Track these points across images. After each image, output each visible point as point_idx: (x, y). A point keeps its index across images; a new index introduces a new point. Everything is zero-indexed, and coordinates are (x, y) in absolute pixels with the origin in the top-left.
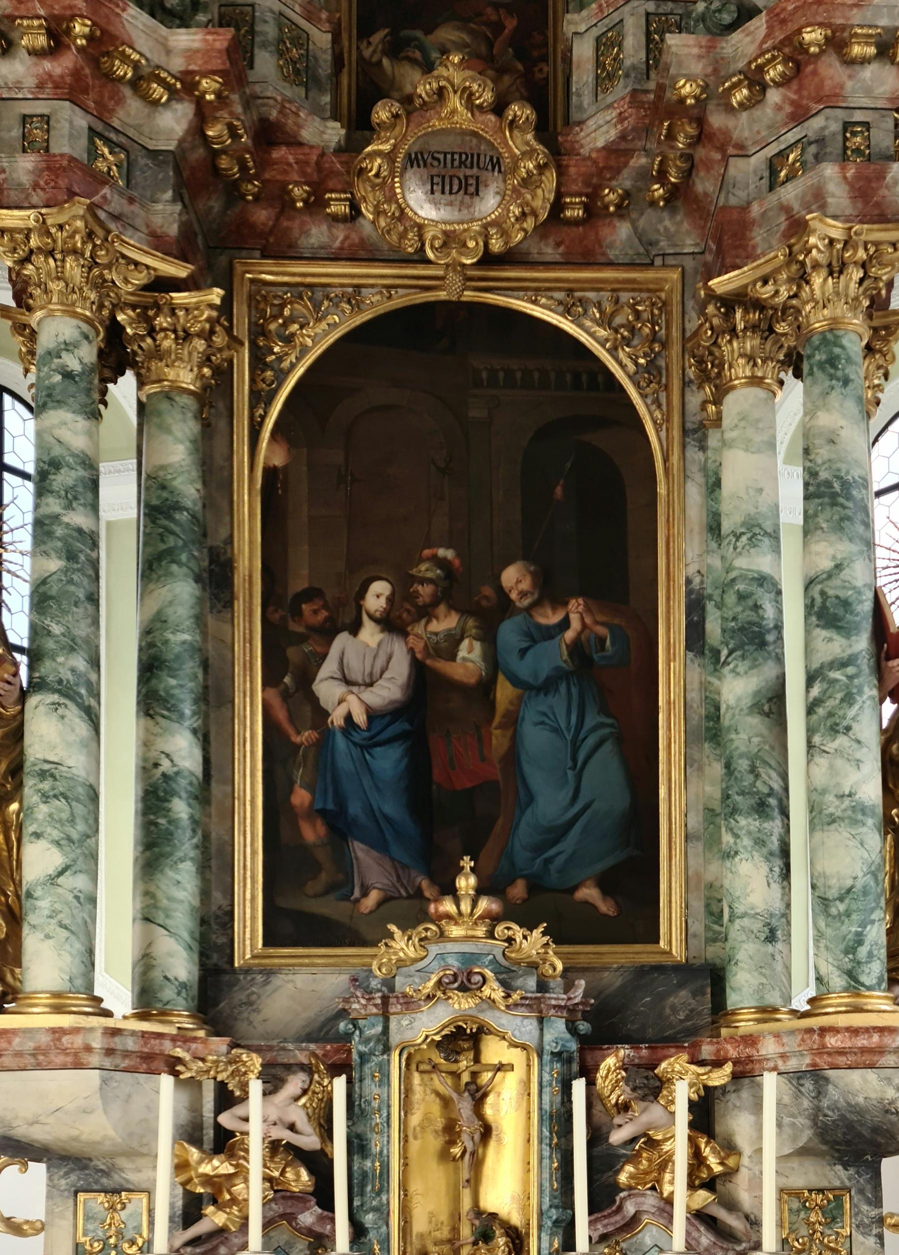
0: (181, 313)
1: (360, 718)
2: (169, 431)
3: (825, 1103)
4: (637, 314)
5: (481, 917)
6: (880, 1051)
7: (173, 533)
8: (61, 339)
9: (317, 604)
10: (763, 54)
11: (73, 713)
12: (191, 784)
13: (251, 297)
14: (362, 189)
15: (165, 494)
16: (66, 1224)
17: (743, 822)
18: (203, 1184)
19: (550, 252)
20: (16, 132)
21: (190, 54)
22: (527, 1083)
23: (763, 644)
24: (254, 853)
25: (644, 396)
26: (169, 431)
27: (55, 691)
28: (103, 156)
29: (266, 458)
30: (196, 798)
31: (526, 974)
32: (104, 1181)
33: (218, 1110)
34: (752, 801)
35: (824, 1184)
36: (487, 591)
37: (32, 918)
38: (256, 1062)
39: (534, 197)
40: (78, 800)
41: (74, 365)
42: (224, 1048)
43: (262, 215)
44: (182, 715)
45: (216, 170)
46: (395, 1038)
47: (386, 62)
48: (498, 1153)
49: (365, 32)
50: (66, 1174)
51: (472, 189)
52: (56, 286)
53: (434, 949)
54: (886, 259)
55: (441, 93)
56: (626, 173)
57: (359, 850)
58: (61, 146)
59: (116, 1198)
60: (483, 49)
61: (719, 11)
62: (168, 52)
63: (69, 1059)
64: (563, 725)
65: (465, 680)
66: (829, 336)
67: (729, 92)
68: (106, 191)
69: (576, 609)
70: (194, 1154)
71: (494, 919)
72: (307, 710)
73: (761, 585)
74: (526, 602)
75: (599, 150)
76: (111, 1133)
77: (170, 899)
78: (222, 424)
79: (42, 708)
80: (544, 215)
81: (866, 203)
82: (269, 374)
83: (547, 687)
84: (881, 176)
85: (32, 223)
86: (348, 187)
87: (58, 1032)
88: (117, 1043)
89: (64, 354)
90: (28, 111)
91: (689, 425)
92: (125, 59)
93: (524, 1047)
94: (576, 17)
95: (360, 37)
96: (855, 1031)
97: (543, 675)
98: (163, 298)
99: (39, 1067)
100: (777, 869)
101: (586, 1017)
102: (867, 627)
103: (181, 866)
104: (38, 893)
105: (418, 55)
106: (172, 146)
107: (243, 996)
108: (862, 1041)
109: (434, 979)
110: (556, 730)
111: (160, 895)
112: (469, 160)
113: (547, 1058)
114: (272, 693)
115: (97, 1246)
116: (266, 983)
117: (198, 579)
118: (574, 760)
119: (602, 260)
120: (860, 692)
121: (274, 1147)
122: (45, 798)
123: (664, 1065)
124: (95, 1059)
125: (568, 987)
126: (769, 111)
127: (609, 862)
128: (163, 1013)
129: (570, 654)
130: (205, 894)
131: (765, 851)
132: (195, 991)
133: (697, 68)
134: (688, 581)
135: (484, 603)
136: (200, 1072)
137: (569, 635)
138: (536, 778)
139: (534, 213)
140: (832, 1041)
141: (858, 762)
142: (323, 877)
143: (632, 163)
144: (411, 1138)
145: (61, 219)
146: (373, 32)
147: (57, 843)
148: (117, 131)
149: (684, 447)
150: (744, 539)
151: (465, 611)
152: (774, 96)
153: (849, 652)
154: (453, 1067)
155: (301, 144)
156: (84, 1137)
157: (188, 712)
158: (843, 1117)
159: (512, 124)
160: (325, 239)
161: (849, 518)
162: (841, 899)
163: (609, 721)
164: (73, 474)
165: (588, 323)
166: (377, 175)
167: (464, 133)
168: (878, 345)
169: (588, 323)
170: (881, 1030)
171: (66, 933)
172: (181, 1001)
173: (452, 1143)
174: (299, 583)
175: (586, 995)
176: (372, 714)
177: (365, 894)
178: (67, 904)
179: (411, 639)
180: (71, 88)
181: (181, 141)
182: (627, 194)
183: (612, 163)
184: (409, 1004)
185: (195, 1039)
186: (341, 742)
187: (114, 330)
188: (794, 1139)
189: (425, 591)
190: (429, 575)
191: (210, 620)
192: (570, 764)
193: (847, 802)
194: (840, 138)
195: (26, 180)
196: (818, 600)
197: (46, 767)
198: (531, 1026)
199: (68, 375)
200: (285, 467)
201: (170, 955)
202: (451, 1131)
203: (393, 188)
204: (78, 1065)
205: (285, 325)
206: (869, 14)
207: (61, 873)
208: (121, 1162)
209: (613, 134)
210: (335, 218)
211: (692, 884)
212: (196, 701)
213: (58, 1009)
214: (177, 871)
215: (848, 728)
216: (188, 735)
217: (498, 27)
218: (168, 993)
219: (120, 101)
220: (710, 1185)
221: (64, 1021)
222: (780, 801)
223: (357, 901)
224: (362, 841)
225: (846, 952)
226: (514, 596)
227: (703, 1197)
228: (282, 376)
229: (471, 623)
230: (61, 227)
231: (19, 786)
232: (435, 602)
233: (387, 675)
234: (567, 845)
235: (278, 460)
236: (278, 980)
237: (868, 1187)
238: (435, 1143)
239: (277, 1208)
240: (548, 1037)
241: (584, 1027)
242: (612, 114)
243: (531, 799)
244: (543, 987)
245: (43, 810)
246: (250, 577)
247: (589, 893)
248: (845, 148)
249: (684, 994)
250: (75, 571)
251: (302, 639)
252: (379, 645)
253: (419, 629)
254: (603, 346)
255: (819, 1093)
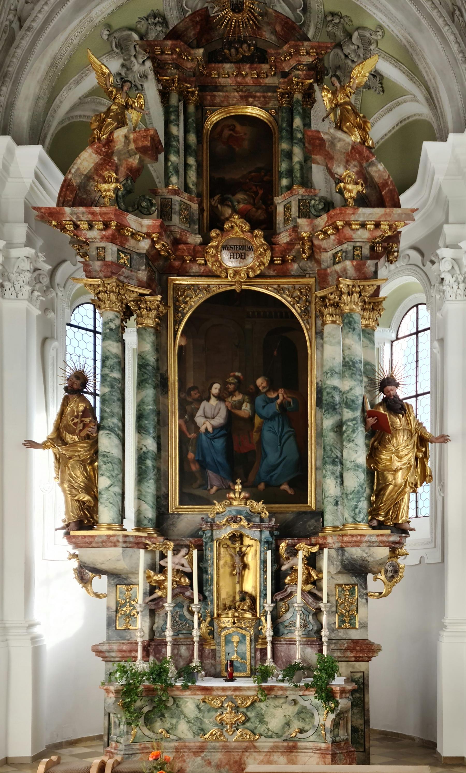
0: (148, 303)
1: (210, 429)
2: (145, 340)
3: (344, 558)
4: (301, 293)
5: (243, 499)
6: (361, 542)
7: (146, 373)
8: (109, 318)
9: (196, 391)
10: (326, 227)
11: (113, 436)
12: (153, 455)
13: (174, 289)
14: (208, 258)
15: (144, 361)
16: (113, 595)
17: (328, 466)
18: (155, 583)
19: (272, 273)
20: (95, 253)
21: (148, 227)
22: (256, 551)
23: (335, 409)
24: (176, 474)
25: (303, 321)
26: (145, 340)
27: (107, 430)
28: (122, 258)
29: (179, 342)
30: (154, 459)
31: (257, 517)
32: (125, 581)
33: (160, 560)
34: (331, 460)
35: (349, 583)
36: (252, 387)
37: (101, 500)
38: (171, 544)
39: (263, 258)
40: (115, 464)
41: (113, 326)
42: (162, 540)
43: (177, 263)
44: (149, 433)
45: (161, 255)
46: (215, 537)
47: (219, 206)
48: (249, 572)
49: (212, 196)
50: (113, 580)
51: (243, 257)
52: (108, 303)
53: (228, 509)
54: (366, 290)
55: (232, 227)
56: (293, 251)
57: (210, 473)
58: (109, 258)
59: (129, 587)
60: (252, 201)
61: (318, 205)
62: (142, 226)
63: (113, 544)
64: (277, 431)
65: (244, 416)
66: (349, 315)
67: (319, 235)
68: (123, 269)
69: (281, 392)
70: (152, 573)
71: (246, 499)
72: (193, 427)
73: (334, 390)
74: (265, 390)
75: (285, 243)
76: (126, 567)
77: (146, 492)
78: (164, 332)
79: (104, 435)
80: (267, 264)
81: (360, 272)
82: (180, 314)
83: (271, 418)
84: (365, 264)
85: (100, 283)
86: (203, 256)
87: (109, 536)
88: (127, 539)
89: (110, 323)
90: (98, 246)
91: (318, 331)
92: (128, 231)
93: (255, 540)
94: (277, 198)
95: (210, 198)
96: (352, 536)
97: (270, 415)
98: (142, 298)
99: (103, 546)
100: (339, 482)
101: (277, 529)
102: (360, 408)
103: (150, 481)
104: (103, 493)
105: (230, 203)
106: (145, 252)
107: (171, 522)
108: (355, 539)
109: (226, 519)
110: (275, 433)
111: (143, 491)
112: (242, 247)
113: (262, 543)
114: (181, 420)
115: (123, 602)
116: (178, 518)
117: (155, 388)
118: (280, 442)
119: (289, 275)
120: (357, 429)
121: (177, 572)
122: (105, 463)
123: (298, 546)
124: (120, 544)
125: (270, 520)
126: (332, 241)
127: (292, 477)
128: (144, 528)
129: (279, 408)
130: (158, 489)
131: (334, 476)
132: (155, 521)
133: (307, 229)
134: (317, 384)
135: (251, 391)
136: (154, 548)
137: (279, 401)
138: (268, 449)
139: (264, 264)
140: (345, 539)
141: (356, 451)
142: (199, 482)
143: (296, 247)
144: (220, 568)
145: (109, 282)
146: (215, 196)
147: (109, 477)
148: (127, 249)
149: (316, 338)
150: (329, 374)
151: (244, 393)
152: (332, 237)
153: (354, 416)
154: (234, 546)
155: (188, 244)
156: (118, 568)
157: (151, 431)
158: (350, 562)
159: (256, 236)
160: (198, 270)
161: (354, 374)
162: (351, 494)
163: (292, 430)
164: (113, 361)
165: (285, 296)
166: (212, 253)
167: (240, 238)
168: (376, 308)
169: (285, 296)
170: (361, 535)
171: (111, 505)
172: (150, 524)
173: (234, 570)
174: (190, 384)
175: (276, 522)
176: (214, 428)
177: (212, 487)
178: (112, 496)
179: (227, 403)
180: (112, 239)
181: (147, 250)
182: (294, 257)
183: (289, 247)
184: (219, 527)
185: (153, 537)
186: (204, 437)
187: (128, 307)
188: (337, 569)
189: (231, 387)
190: (233, 381)
191: (161, 398)
192: (279, 444)
193: (353, 464)
194: (352, 251)
195: (98, 269)
196: (345, 399)
197: (105, 453)
198: (257, 533)
199: (111, 330)
200: (185, 346)
201: (146, 510)
202: (233, 567)
203: (218, 257)
204: (115, 546)
205: (185, 298)
206: (357, 216)
207: (110, 487)
208: (130, 576)
209: (288, 239)
210: (200, 265)
211: (318, 485)
212: (155, 428)
213: (109, 529)
214: (148, 483)
215: (353, 441)
216: (152, 439)
217: (256, 193)
218: (146, 522)
219: (127, 241)
220: (314, 583)
221: (111, 533)
222: (340, 460)
223: (209, 490)
224: (211, 470)
225: (352, 511)
226: (260, 388)
227: (309, 587)
228: (184, 315)
229: (246, 397)
230: (109, 284)
231: (97, 458)
232: (235, 391)
233: (219, 415)
234: (278, 471)
235: (183, 343)
236: (182, 517)
237: (363, 584)
238: (228, 570)
239: (178, 590)
240: (263, 537)
241: (276, 533)
242: (287, 234)
243: (266, 455)
244: (262, 520)
245: (104, 467)
246: (174, 383)
247: (285, 487)
248: (354, 254)
249: (313, 521)
250: (113, 391)
251: (191, 403)
252: (216, 405)
253: (229, 399)
254: (290, 303)
255: (343, 555)
